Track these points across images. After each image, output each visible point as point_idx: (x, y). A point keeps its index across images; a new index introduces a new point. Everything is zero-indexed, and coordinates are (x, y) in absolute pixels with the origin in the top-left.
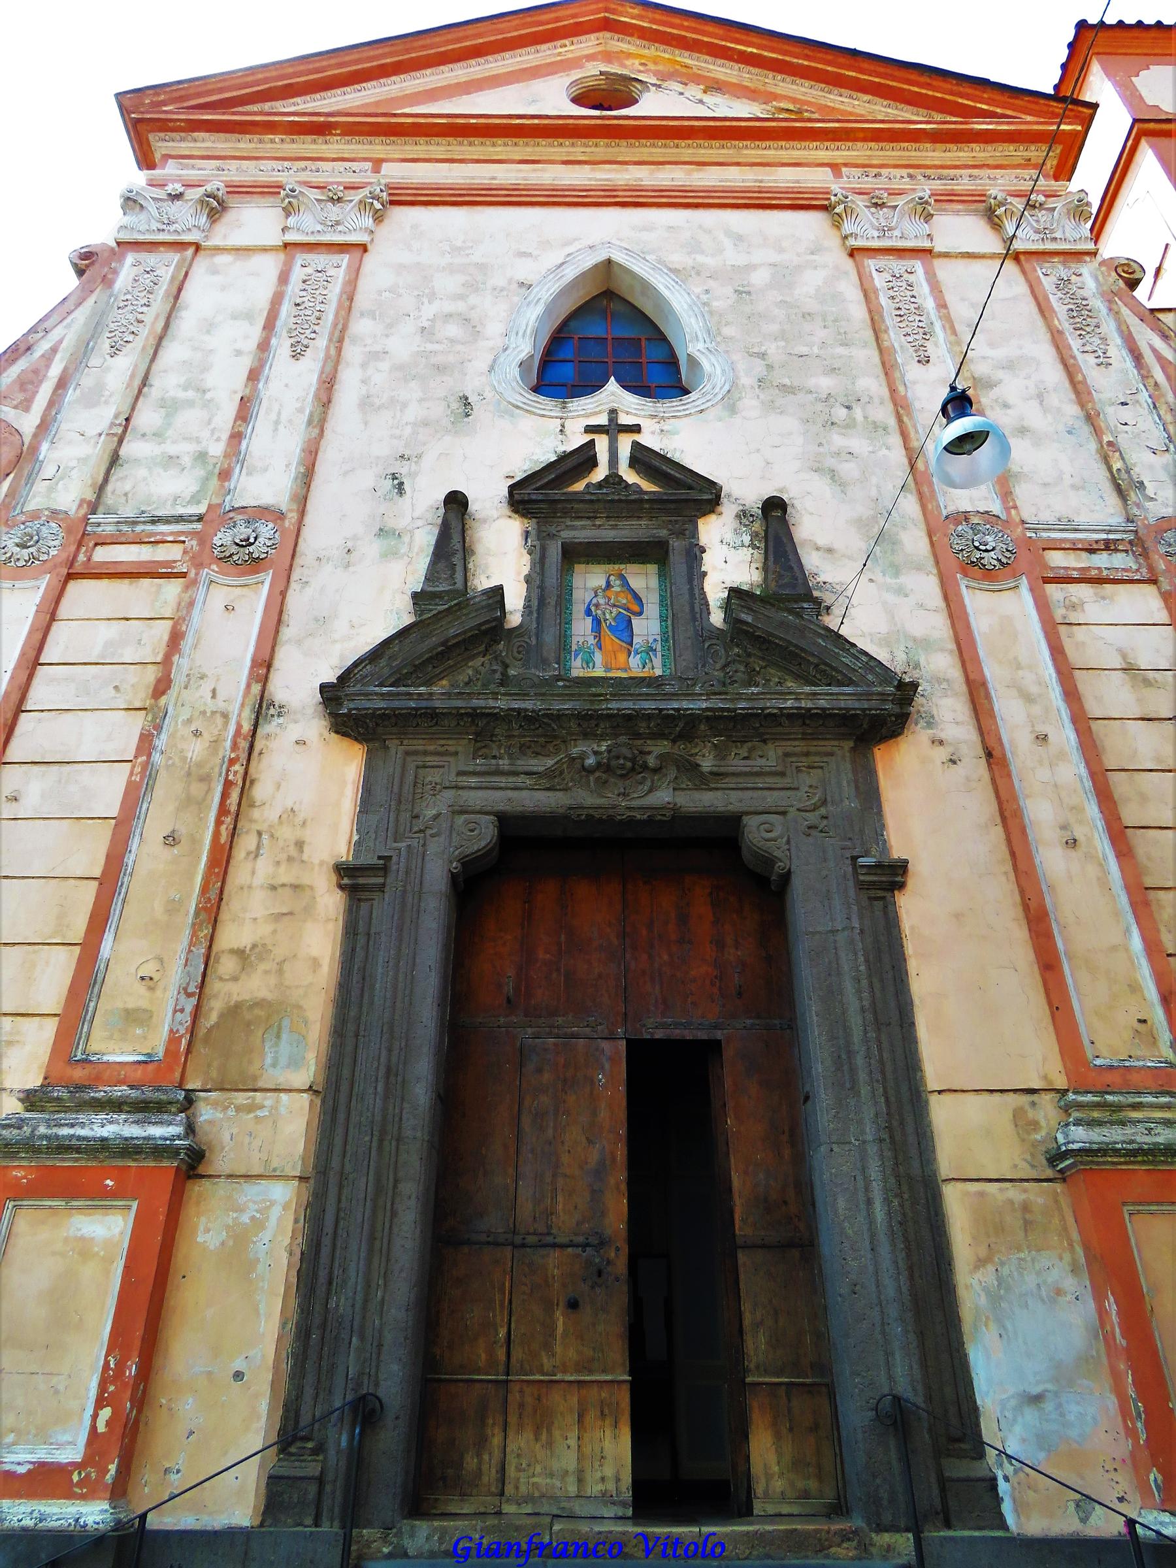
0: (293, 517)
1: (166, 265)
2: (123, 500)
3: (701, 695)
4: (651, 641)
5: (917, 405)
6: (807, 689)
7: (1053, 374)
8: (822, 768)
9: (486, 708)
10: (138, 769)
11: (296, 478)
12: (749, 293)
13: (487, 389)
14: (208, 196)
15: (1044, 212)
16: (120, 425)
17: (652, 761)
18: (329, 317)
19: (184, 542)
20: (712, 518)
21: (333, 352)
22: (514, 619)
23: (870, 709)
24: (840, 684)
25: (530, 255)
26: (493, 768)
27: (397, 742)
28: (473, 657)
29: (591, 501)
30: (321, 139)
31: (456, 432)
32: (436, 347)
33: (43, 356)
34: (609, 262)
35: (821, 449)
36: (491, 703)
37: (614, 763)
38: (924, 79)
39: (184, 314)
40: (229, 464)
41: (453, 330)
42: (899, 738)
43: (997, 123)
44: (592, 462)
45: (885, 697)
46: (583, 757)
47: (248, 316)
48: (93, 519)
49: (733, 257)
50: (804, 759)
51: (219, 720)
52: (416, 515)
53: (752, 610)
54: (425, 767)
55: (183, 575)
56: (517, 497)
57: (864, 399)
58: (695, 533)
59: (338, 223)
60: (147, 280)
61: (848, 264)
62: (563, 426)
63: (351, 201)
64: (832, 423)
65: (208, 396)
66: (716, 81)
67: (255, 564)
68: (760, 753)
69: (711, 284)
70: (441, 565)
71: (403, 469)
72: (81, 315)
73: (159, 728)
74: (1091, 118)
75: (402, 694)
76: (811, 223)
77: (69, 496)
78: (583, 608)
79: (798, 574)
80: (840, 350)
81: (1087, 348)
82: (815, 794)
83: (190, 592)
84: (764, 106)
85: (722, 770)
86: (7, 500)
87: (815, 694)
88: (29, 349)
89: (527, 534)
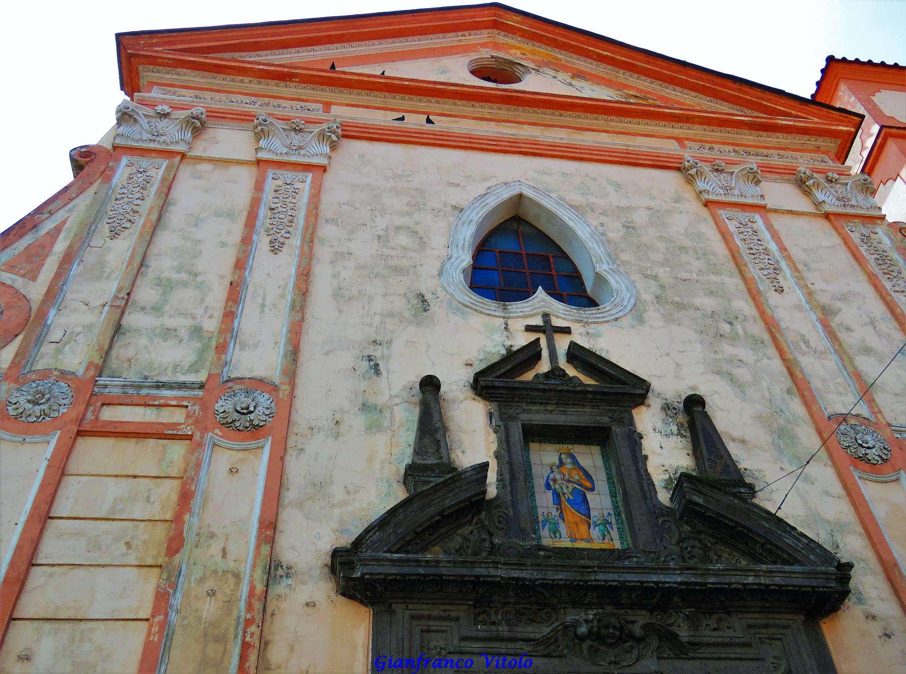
0: (284, 390)
1: (158, 170)
2: (126, 365)
3: (676, 569)
4: (606, 514)
5: (783, 325)
6: (764, 567)
7: (878, 309)
8: (780, 639)
9: (488, 576)
10: (155, 629)
11: (285, 355)
12: (634, 228)
13: (439, 289)
14: (193, 118)
15: (839, 186)
16: (123, 298)
17: (637, 630)
18: (301, 221)
19: (187, 407)
20: (643, 409)
21: (306, 249)
22: (492, 492)
23: (818, 587)
24: (785, 562)
25: (458, 185)
26: (494, 634)
27: (403, 606)
28: (462, 526)
29: (544, 390)
30: (282, 84)
31: (418, 324)
32: (391, 252)
33: (48, 233)
34: (521, 196)
35: (717, 356)
36: (493, 572)
37: (603, 631)
38: (737, 86)
39: (173, 208)
40: (225, 339)
41: (404, 239)
42: (839, 612)
43: (794, 121)
44: (538, 356)
45: (830, 577)
46: (575, 625)
47: (231, 215)
48: (101, 381)
49: (616, 199)
50: (764, 630)
51: (231, 580)
52: (394, 393)
53: (703, 494)
54: (428, 631)
55: (189, 438)
56: (481, 383)
57: (741, 318)
58: (631, 422)
59: (301, 148)
60: (140, 178)
61: (705, 212)
62: (506, 324)
63: (311, 132)
64: (721, 336)
65: (199, 278)
66: (581, 71)
67: (255, 430)
68: (727, 624)
69: (603, 219)
70: (427, 441)
71: (377, 353)
72: (82, 203)
73: (174, 586)
74: (861, 123)
75: (411, 561)
76: (669, 180)
77: (76, 359)
78: (542, 482)
79: (729, 462)
80: (713, 278)
81: (897, 288)
82: (780, 665)
83: (196, 454)
84: (618, 92)
85: (698, 640)
86: (17, 360)
87: (771, 572)
88: (35, 227)
89: (491, 415)
